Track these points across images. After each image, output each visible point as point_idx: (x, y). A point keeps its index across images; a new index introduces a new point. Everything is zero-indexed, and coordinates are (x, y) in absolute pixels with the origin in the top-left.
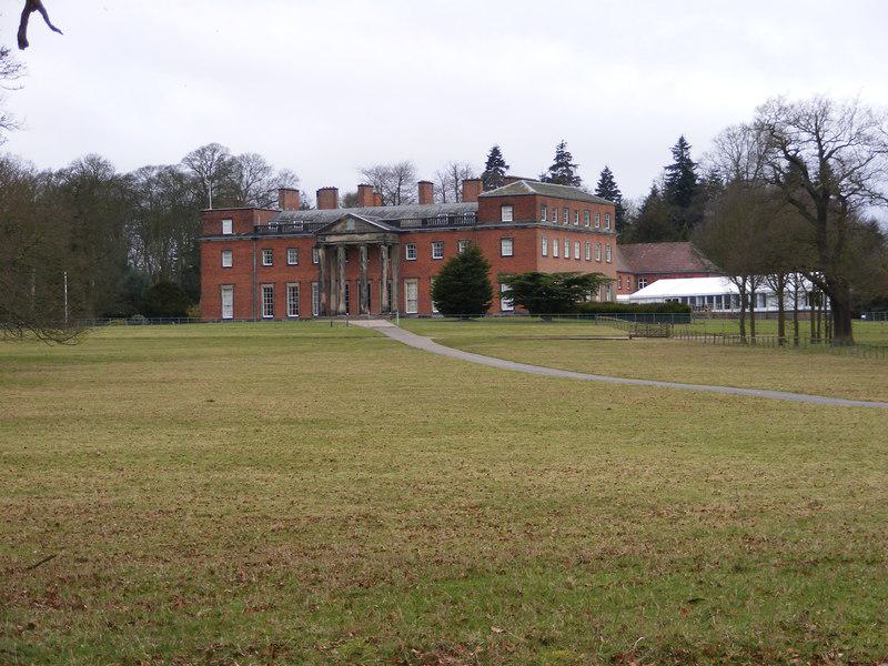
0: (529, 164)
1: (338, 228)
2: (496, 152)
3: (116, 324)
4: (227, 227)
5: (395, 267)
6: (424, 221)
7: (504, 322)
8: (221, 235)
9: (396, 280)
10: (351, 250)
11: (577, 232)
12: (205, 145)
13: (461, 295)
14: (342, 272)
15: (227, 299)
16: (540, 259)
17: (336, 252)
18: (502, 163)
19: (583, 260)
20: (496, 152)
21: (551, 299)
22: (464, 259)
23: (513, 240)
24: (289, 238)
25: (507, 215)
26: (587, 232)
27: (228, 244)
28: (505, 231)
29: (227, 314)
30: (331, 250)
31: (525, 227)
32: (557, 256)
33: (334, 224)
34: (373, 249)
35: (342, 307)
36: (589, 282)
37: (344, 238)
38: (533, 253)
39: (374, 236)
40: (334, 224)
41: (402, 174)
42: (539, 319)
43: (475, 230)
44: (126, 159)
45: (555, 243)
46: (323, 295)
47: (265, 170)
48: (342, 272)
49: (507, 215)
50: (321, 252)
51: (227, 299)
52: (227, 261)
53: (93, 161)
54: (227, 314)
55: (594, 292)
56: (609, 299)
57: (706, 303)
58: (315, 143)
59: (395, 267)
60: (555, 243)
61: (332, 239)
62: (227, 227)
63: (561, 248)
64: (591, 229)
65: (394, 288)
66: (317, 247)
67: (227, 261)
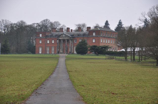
0: (105, 23)
1: (61, 36)
2: (107, 22)
3: (24, 54)
4: (41, 35)
5: (72, 44)
6: (78, 35)
7: (91, 56)
8: (40, 37)
9: (72, 46)
10: (64, 40)
11: (104, 37)
12: (45, 19)
13: (82, 50)
14: (62, 45)
15: (40, 49)
16: (100, 43)
17: (61, 41)
18: (108, 24)
19: (108, 43)
20: (107, 22)
21: (100, 51)
22: (81, 42)
23: (95, 39)
24: (52, 38)
25: (94, 34)
26: (111, 38)
27: (41, 39)
28: (94, 37)
29: (40, 53)
30: (60, 40)
31: (97, 37)
32: (103, 42)
33: (61, 35)
34: (68, 40)
35: (62, 52)
36: (106, 47)
37: (62, 38)
38: (99, 42)
39: (68, 38)
40: (61, 35)
41: (84, 25)
42: (80, 54)
43: (88, 37)
44: (29, 22)
45: (104, 40)
46: (58, 49)
47: (59, 24)
48: (62, 45)
49: (94, 34)
50: (58, 41)
51: (40, 49)
52: (41, 42)
53: (22, 22)
54: (40, 53)
55: (107, 49)
56: (116, 51)
57: (48, 49)
58: (69, 20)
59: (72, 44)
60: (104, 40)
61: (60, 38)
62: (41, 35)
63: (105, 41)
64: (112, 37)
65: (72, 48)
66: (57, 40)
67: (41, 42)
